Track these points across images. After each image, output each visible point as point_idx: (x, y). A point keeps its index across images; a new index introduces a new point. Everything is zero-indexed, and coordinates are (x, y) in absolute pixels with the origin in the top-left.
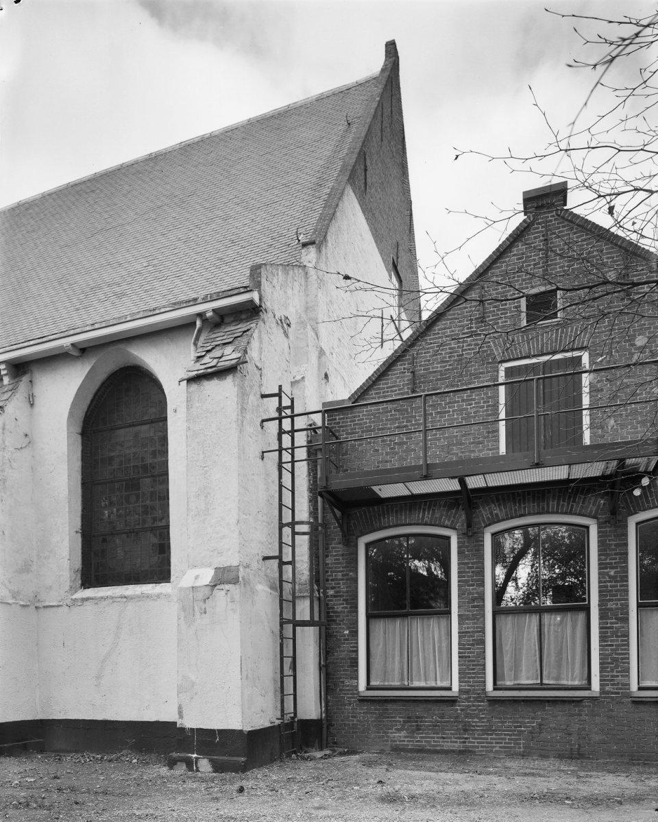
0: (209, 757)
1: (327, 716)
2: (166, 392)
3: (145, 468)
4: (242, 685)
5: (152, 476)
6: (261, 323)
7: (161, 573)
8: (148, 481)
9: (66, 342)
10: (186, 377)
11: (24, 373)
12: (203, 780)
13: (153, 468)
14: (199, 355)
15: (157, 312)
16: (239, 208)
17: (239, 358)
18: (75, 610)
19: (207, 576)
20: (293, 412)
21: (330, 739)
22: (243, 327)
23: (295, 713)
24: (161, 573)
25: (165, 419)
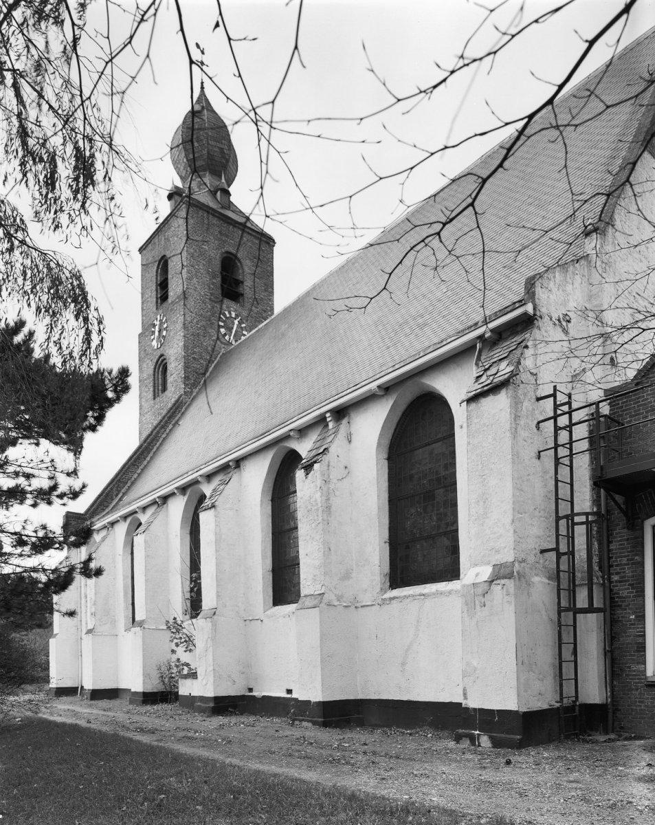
0: (490, 734)
1: (613, 701)
2: (453, 411)
3: (438, 480)
4: (517, 670)
5: (445, 487)
6: (535, 331)
7: (453, 572)
8: (441, 491)
9: (374, 386)
10: (465, 398)
11: (344, 417)
12: (481, 754)
13: (446, 479)
14: (478, 375)
15: (445, 343)
16: (532, 209)
17: (512, 371)
18: (385, 607)
19: (486, 572)
20: (570, 407)
21: (616, 723)
22: (518, 339)
23: (577, 697)
24: (453, 572)
25: (453, 435)
